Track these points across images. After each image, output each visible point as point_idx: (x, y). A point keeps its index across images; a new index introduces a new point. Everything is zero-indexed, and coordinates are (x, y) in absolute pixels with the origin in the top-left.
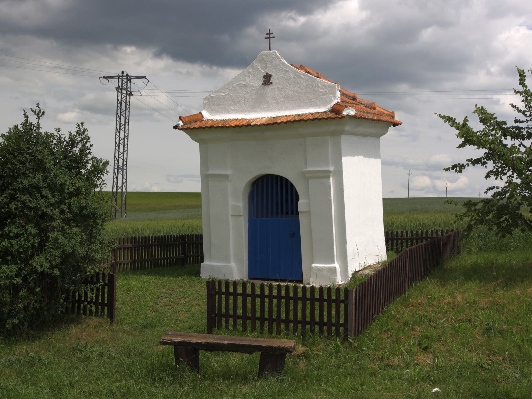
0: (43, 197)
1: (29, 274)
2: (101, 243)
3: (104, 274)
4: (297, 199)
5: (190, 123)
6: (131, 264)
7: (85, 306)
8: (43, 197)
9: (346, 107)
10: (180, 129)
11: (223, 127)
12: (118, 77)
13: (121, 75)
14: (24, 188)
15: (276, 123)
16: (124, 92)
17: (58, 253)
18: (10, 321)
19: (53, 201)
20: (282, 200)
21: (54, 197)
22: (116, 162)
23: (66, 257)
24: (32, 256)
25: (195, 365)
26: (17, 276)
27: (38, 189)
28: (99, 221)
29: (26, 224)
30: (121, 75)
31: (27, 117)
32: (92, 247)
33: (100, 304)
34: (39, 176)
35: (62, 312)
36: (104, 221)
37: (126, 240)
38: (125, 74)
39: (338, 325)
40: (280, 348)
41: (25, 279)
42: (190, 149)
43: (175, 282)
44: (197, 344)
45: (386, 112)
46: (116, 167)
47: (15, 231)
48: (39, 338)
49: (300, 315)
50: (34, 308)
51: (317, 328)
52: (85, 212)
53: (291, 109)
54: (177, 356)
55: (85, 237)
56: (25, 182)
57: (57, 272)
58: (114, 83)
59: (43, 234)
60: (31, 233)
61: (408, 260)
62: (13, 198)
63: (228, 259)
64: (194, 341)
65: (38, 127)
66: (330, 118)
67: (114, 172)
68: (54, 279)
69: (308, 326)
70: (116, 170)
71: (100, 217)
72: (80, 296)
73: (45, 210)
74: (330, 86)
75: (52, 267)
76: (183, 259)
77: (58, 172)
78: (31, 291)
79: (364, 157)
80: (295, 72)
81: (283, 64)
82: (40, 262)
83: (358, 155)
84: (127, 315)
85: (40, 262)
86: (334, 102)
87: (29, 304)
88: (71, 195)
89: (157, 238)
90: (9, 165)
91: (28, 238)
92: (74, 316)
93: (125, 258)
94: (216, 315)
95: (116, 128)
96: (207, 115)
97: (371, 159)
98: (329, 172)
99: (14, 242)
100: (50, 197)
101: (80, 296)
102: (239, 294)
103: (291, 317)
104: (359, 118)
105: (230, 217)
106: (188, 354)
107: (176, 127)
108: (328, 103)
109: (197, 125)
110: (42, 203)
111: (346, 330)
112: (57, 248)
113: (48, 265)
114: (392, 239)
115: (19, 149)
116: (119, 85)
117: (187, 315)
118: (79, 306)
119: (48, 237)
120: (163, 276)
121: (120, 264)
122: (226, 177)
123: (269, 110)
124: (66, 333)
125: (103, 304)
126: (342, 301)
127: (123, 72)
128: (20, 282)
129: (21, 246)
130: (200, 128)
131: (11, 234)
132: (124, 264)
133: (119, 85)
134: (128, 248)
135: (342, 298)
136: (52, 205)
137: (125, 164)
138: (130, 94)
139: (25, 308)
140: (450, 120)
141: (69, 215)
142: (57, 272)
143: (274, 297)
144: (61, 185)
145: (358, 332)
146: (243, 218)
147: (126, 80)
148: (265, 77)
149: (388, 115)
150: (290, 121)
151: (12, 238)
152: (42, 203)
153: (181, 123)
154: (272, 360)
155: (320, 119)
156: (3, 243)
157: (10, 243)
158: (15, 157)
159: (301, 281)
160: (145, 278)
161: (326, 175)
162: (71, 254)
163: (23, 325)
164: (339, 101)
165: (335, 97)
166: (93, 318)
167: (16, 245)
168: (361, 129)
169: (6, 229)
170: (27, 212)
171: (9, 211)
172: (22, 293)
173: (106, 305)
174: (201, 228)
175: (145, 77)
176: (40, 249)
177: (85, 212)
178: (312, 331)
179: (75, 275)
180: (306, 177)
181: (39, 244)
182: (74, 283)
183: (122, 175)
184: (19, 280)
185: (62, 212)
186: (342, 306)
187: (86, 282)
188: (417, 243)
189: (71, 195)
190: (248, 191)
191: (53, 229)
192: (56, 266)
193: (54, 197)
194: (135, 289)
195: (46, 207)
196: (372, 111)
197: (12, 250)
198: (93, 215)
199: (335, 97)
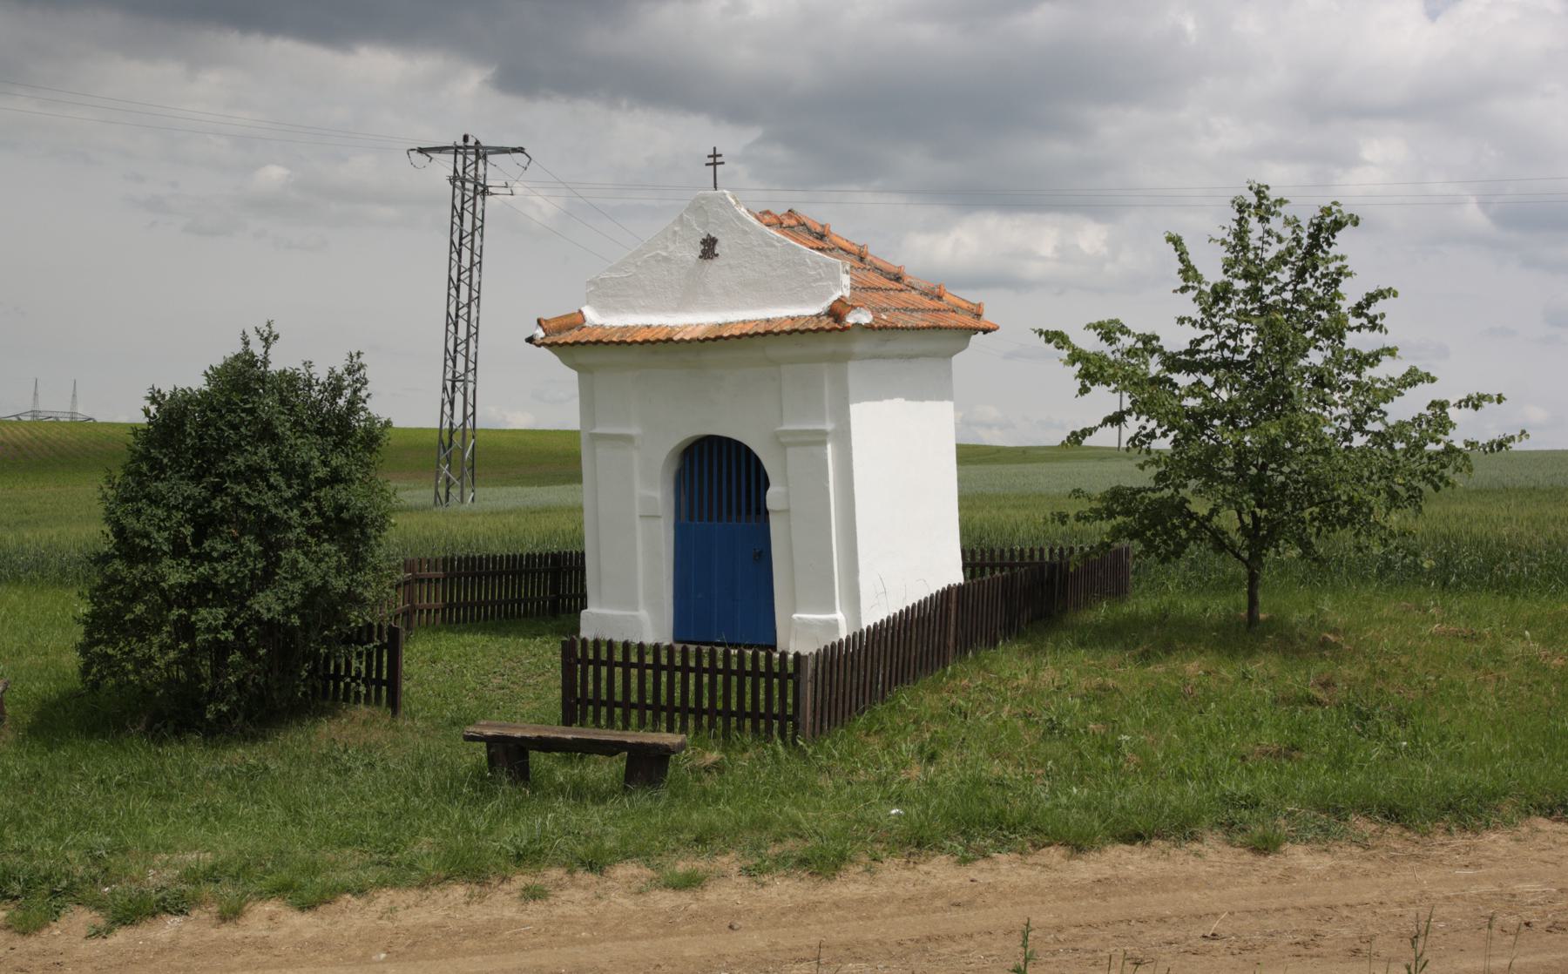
0: (271, 487)
1: (248, 623)
2: (375, 569)
3: (380, 627)
4: (767, 485)
5: (559, 331)
6: (444, 611)
7: (347, 685)
8: (271, 487)
9: (853, 307)
10: (539, 346)
11: (620, 343)
12: (456, 150)
13: (460, 143)
14: (238, 473)
15: (721, 337)
16: (469, 186)
17: (297, 586)
18: (212, 707)
19: (288, 494)
20: (748, 485)
21: (290, 487)
22: (450, 363)
23: (314, 596)
24: (251, 593)
25: (522, 774)
26: (225, 627)
27: (261, 472)
28: (371, 531)
29: (242, 535)
30: (460, 143)
31: (247, 343)
32: (359, 577)
33: (374, 681)
34: (264, 451)
35: (304, 694)
36: (381, 528)
37: (433, 564)
38: (471, 142)
39: (783, 717)
40: (655, 746)
41: (239, 632)
42: (562, 379)
43: (526, 646)
44: (524, 739)
45: (965, 305)
46: (449, 376)
47: (221, 547)
48: (265, 739)
49: (664, 679)
50: (256, 685)
51: (748, 723)
52: (345, 515)
53: (752, 307)
54: (492, 760)
55: (344, 559)
56: (240, 461)
57: (295, 620)
58: (444, 166)
59: (271, 551)
60: (249, 552)
61: (953, 606)
62: (218, 490)
63: (633, 602)
64: (518, 734)
65: (266, 362)
66: (822, 329)
67: (445, 389)
68: (291, 632)
69: (734, 720)
70: (449, 384)
71: (373, 522)
72: (337, 667)
73: (274, 511)
74: (827, 265)
75: (288, 612)
76: (554, 603)
77: (299, 441)
78: (249, 653)
79: (909, 398)
80: (762, 234)
81: (740, 218)
82: (267, 604)
83: (891, 398)
84: (426, 703)
85: (267, 604)
86: (835, 297)
87: (246, 675)
88: (321, 483)
89: (513, 559)
90: (212, 431)
91: (244, 560)
92: (327, 704)
93: (430, 598)
94: (578, 701)
95: (450, 278)
96: (592, 316)
97: (927, 403)
98: (824, 433)
99: (219, 567)
100: (284, 487)
101: (337, 667)
102: (617, 664)
103: (604, 671)
104: (880, 329)
105: (638, 522)
106: (511, 756)
107: (530, 340)
108: (824, 298)
109: (570, 337)
110: (269, 498)
111: (796, 726)
112: (294, 578)
113: (279, 608)
114: (973, 561)
115: (228, 402)
116: (455, 170)
117: (536, 705)
118: (337, 687)
119: (279, 559)
120: (507, 635)
121: (421, 611)
122: (628, 439)
123: (711, 308)
124: (311, 730)
125: (379, 682)
126: (790, 676)
127: (466, 138)
128: (232, 637)
129: (233, 575)
130: (576, 343)
131: (215, 554)
132: (429, 611)
133: (455, 170)
134: (437, 580)
135: (790, 669)
136: (286, 501)
137: (472, 368)
138: (485, 192)
139: (240, 685)
140: (1056, 338)
141: (317, 520)
142: (295, 620)
143: (677, 669)
144: (303, 466)
145: (818, 731)
146: (661, 522)
147: (473, 158)
148: (704, 242)
149: (970, 311)
150: (747, 335)
151: (217, 560)
152: (269, 498)
153: (540, 333)
154: (647, 767)
155: (803, 332)
156: (201, 569)
157: (214, 569)
158: (222, 417)
159: (774, 648)
160: (468, 638)
161: (819, 439)
162: (318, 589)
163: (236, 716)
164: (847, 293)
165: (838, 285)
166: (362, 706)
167: (223, 573)
168: (894, 346)
169: (206, 544)
170: (242, 514)
171: (210, 514)
172: (235, 657)
173: (384, 683)
174: (581, 541)
175: (520, 150)
176: (265, 579)
177: (345, 515)
178: (740, 728)
179: (328, 627)
180: (782, 442)
181: (264, 569)
182: (325, 640)
183: (465, 395)
184: (228, 635)
185: (305, 513)
186: (790, 684)
187: (348, 641)
188: (992, 573)
189: (321, 483)
190: (673, 468)
191: (288, 546)
192: (294, 610)
193: (290, 487)
194: (447, 658)
195: (276, 506)
196: (936, 304)
197: (218, 580)
198: (360, 521)
199: (838, 285)
